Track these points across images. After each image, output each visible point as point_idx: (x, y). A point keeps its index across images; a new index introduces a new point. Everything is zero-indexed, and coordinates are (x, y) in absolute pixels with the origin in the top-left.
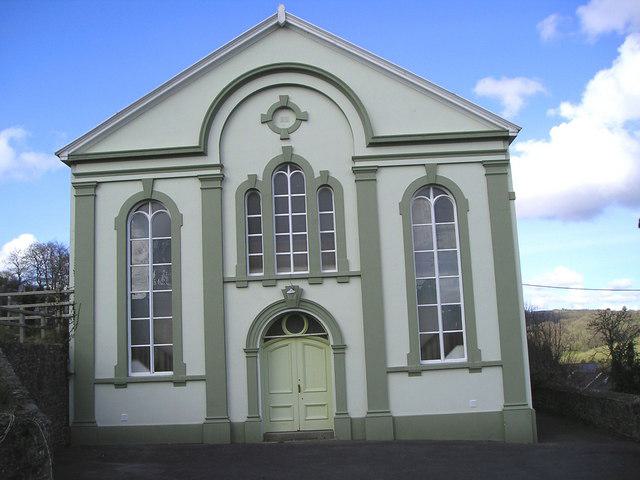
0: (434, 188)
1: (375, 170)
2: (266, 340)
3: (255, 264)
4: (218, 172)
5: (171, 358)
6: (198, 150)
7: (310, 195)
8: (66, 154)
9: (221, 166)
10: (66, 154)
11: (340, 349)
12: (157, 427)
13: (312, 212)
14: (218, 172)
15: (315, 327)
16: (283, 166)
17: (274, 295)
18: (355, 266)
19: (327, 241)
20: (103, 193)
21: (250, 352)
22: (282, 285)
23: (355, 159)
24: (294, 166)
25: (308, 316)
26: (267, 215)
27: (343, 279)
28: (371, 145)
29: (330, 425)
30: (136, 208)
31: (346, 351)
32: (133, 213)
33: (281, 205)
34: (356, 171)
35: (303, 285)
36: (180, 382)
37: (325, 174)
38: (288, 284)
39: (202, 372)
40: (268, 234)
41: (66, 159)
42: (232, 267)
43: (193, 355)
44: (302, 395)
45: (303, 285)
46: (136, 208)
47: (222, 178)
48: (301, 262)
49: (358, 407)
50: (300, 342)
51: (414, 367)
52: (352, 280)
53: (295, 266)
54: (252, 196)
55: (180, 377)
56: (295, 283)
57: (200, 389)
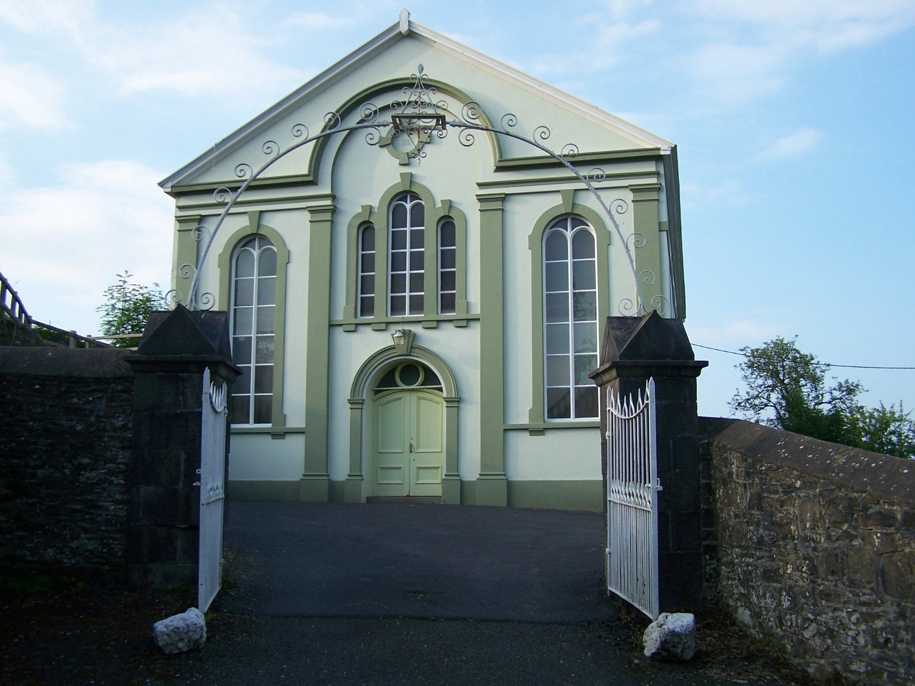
0: (573, 219)
1: (505, 198)
2: (377, 392)
3: (367, 307)
4: (329, 202)
5: (269, 408)
6: (310, 178)
7: (430, 229)
8: (170, 185)
9: (333, 197)
10: (170, 185)
11: (455, 402)
12: (252, 483)
13: (431, 249)
14: (329, 202)
15: (431, 379)
16: (403, 195)
17: (384, 340)
18: (476, 310)
19: (448, 280)
20: (210, 226)
21: (355, 402)
22: (393, 328)
23: (481, 185)
24: (414, 196)
25: (427, 370)
26: (382, 251)
27: (466, 322)
28: (499, 169)
29: (437, 491)
30: (549, 226)
31: (462, 405)
32: (238, 250)
33: (397, 240)
34: (482, 199)
35: (417, 329)
36: (279, 435)
37: (449, 204)
38: (400, 327)
39: (447, 125)
40: (381, 273)
41: (169, 190)
42: (343, 308)
43: (295, 415)
44: (413, 455)
45: (417, 329)
46: (549, 226)
47: (334, 211)
48: (417, 305)
49: (471, 469)
50: (414, 397)
51: (540, 425)
52: (472, 324)
53: (410, 309)
54: (366, 229)
55: (280, 429)
56: (407, 327)
57: (297, 444)
